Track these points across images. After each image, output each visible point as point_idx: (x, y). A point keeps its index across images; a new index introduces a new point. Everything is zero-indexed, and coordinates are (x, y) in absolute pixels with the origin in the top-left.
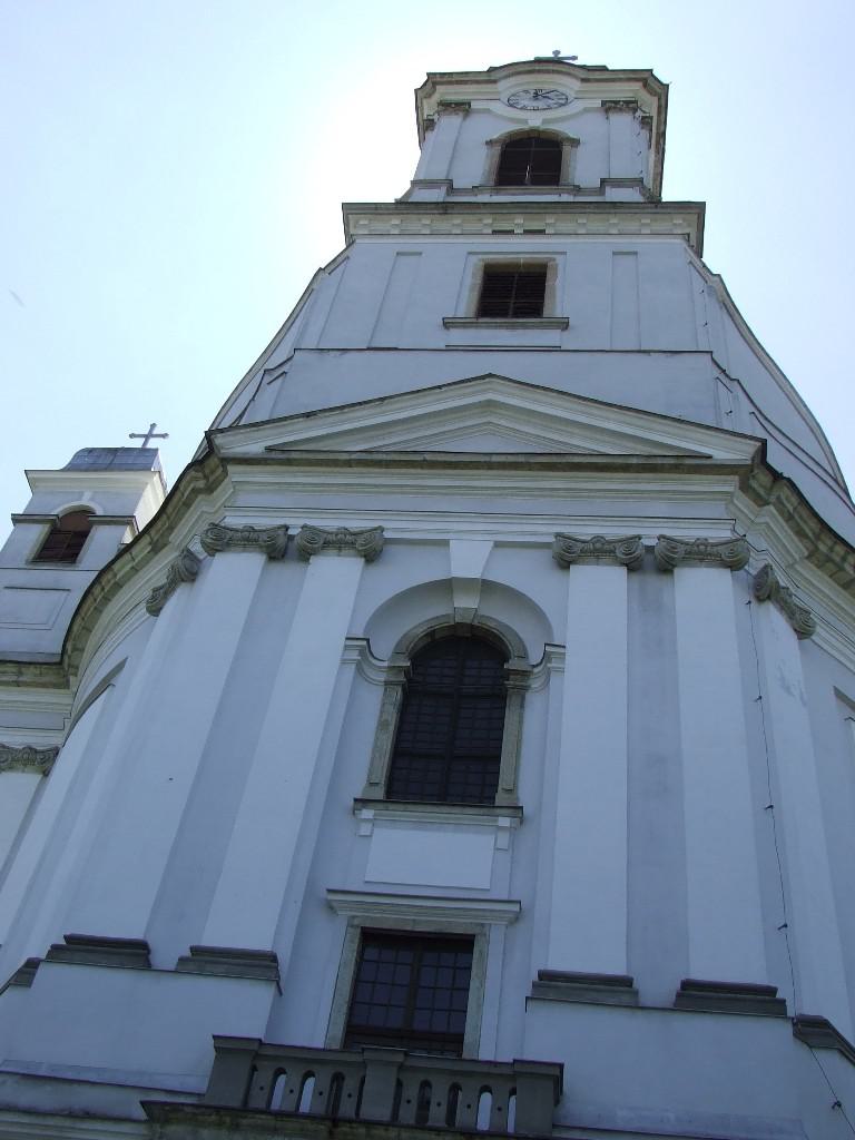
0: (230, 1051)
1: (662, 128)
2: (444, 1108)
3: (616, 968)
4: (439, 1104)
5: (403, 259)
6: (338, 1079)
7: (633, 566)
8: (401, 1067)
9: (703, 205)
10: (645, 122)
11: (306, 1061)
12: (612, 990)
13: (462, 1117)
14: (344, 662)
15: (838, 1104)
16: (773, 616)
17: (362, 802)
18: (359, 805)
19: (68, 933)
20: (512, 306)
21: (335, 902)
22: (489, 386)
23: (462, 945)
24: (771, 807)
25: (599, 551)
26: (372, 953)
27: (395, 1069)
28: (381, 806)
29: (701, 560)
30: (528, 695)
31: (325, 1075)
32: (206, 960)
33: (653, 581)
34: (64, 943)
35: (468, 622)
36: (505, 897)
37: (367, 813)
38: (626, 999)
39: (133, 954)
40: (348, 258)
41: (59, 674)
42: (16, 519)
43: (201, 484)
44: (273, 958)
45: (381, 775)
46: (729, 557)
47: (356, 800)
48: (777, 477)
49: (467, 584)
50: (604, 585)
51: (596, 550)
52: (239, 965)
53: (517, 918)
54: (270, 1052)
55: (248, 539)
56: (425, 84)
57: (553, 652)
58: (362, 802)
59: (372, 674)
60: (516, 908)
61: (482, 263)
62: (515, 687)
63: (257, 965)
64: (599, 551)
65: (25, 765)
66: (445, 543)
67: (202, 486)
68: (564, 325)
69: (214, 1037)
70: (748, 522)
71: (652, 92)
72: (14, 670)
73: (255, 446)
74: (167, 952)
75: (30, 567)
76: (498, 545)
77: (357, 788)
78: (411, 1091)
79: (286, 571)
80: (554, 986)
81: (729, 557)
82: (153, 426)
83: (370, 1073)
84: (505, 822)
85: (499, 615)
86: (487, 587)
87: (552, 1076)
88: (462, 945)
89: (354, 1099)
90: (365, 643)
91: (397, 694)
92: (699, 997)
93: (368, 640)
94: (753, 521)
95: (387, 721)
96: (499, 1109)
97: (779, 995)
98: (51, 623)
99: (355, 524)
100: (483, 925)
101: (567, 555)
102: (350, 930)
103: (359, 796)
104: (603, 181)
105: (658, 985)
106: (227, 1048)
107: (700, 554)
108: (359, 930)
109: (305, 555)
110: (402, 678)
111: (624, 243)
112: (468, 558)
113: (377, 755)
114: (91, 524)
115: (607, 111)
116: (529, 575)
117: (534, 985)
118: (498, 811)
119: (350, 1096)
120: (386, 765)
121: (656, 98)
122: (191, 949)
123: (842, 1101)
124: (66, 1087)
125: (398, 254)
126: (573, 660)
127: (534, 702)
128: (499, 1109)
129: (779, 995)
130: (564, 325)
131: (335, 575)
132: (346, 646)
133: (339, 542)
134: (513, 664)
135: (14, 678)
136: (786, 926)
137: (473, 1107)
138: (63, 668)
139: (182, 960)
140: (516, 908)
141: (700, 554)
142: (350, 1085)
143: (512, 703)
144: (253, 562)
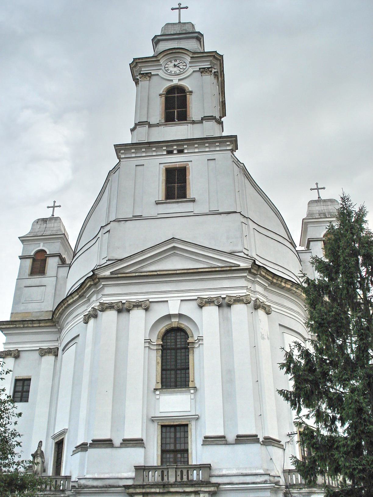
0: (138, 469)
1: (222, 69)
2: (186, 476)
3: (222, 434)
4: (185, 475)
5: (138, 167)
6: (162, 472)
7: (220, 306)
8: (176, 468)
9: (236, 137)
10: (216, 74)
11: (154, 469)
12: (220, 440)
14: (145, 347)
15: (271, 459)
16: (261, 312)
17: (156, 390)
18: (155, 390)
19: (92, 439)
20: (176, 186)
22: (173, 241)
23: (187, 425)
24: (258, 381)
25: (210, 302)
26: (164, 430)
27: (174, 469)
28: (161, 390)
29: (238, 302)
30: (195, 350)
31: (160, 471)
32: (127, 443)
33: (226, 310)
34: (92, 442)
35: (176, 326)
36: (194, 414)
37: (158, 392)
38: (224, 442)
39: (108, 443)
40: (119, 168)
41: (52, 322)
42: (21, 258)
43: (92, 283)
44: (142, 440)
45: (159, 380)
46: (246, 301)
47: (154, 389)
48: (259, 266)
49: (175, 316)
50: (212, 311)
51: (209, 302)
52: (134, 443)
53: (198, 419)
54: (147, 468)
55: (111, 307)
56: (133, 62)
57: (200, 339)
58: (156, 390)
59: (152, 347)
60: (197, 417)
61: (164, 168)
62: (191, 347)
63: (138, 443)
64: (210, 302)
65: (49, 353)
66: (167, 301)
67: (93, 284)
68: (193, 201)
69: (134, 466)
70: (253, 281)
71: (217, 59)
72: (38, 322)
73: (107, 273)
74: (117, 442)
75: (30, 277)
76: (182, 300)
77: (153, 385)
78: (179, 473)
79: (124, 315)
80: (209, 441)
81: (246, 301)
82: (55, 202)
83: (169, 470)
84: (192, 391)
85: (185, 324)
86: (180, 316)
87: (208, 467)
88: (187, 425)
89: (167, 476)
90: (149, 341)
91: (160, 353)
92: (241, 439)
93: (150, 340)
94: (254, 281)
95: (158, 362)
96: (198, 475)
97: (258, 437)
98: (43, 299)
99: (141, 298)
100: (190, 421)
101: (202, 303)
102: (158, 426)
103: (155, 388)
104: (202, 122)
105: (231, 438)
106: (138, 469)
107: (238, 300)
108: (160, 426)
109: (128, 311)
110: (160, 348)
111: (211, 156)
112: (174, 308)
113: (157, 373)
114: (46, 257)
115: (201, 72)
116: (190, 310)
117: (203, 441)
118: (190, 389)
119: (166, 476)
120: (160, 376)
121: (219, 61)
122: (122, 440)
123: (272, 458)
124: (104, 480)
125: (136, 165)
126: (206, 341)
127: (196, 351)
128: (198, 475)
130: (193, 201)
131: (138, 314)
132: (145, 342)
133: (138, 305)
134: (190, 340)
135: (38, 325)
136: (261, 415)
137: (192, 475)
138: (53, 321)
139: (121, 444)
140: (197, 417)
141: (238, 300)
142: (165, 473)
143: (191, 352)
144: (112, 314)
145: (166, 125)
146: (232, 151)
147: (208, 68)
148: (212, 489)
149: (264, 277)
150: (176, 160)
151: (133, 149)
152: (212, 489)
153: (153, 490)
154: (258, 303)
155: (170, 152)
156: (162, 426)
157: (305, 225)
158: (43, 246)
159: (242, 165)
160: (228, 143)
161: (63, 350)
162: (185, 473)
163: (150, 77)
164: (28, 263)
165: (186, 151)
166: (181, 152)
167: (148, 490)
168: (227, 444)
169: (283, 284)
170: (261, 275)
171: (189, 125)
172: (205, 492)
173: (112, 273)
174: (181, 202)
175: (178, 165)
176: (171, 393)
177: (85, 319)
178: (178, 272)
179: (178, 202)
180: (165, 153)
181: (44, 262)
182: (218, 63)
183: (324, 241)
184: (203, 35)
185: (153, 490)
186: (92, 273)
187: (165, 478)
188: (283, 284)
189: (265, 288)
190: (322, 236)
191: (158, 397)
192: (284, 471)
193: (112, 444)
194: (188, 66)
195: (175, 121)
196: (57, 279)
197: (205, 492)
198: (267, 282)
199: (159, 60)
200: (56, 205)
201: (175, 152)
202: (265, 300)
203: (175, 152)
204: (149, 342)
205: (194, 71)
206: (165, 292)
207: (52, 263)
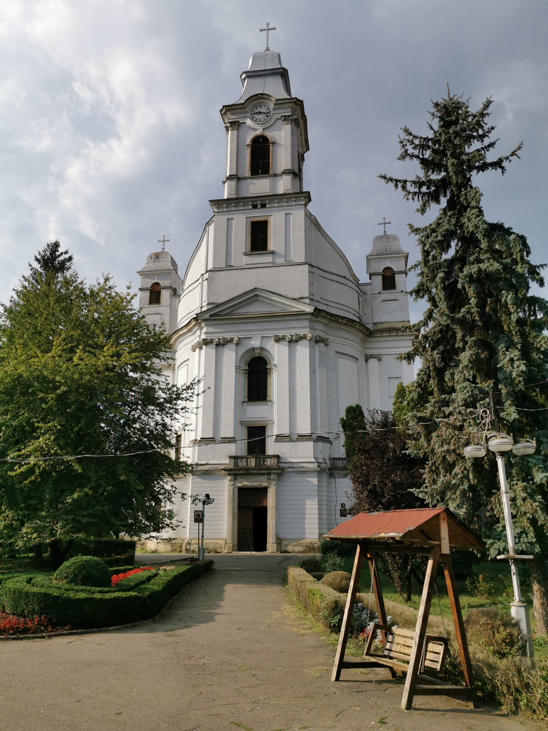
13: (266, 463)
17: (244, 402)
21: (242, 423)
37: (245, 404)
38: (289, 440)
58: (244, 402)
68: (273, 253)
76: (262, 337)
78: (258, 460)
80: (280, 438)
85: (264, 354)
87: (278, 457)
91: (247, 375)
105: (295, 437)
112: (255, 343)
129: (330, 439)
145: (252, 178)
146: (306, 205)
147: (289, 116)
148: (279, 471)
149: (324, 317)
150: (259, 214)
151: (224, 204)
152: (279, 471)
153: (240, 472)
154: (318, 338)
155: (255, 207)
156: (249, 428)
157: (369, 259)
158: (158, 279)
159: (313, 217)
160: (302, 198)
161: (178, 368)
162: (262, 460)
163: (238, 126)
164: (147, 294)
165: (268, 206)
166: (263, 206)
167: (237, 472)
168: (291, 441)
169: (340, 321)
170: (322, 316)
171: (271, 178)
172: (274, 473)
173: (210, 316)
174: (263, 254)
175: (261, 219)
176: (255, 405)
177: (192, 349)
178: (259, 315)
179: (260, 254)
180: (251, 207)
181: (159, 293)
182: (299, 108)
183: (383, 275)
184: (287, 71)
185: (240, 472)
186: (195, 316)
187: (249, 464)
188: (340, 321)
189: (326, 325)
190: (381, 271)
191: (245, 407)
192: (330, 459)
193: (214, 441)
194: (272, 113)
195: (259, 174)
196: (171, 308)
197: (274, 473)
198: (116, 629)
199: (245, 107)
200: (166, 239)
201: (259, 206)
202: (325, 335)
203: (259, 206)
204: (237, 368)
205: (277, 119)
206: (250, 331)
207: (165, 295)
